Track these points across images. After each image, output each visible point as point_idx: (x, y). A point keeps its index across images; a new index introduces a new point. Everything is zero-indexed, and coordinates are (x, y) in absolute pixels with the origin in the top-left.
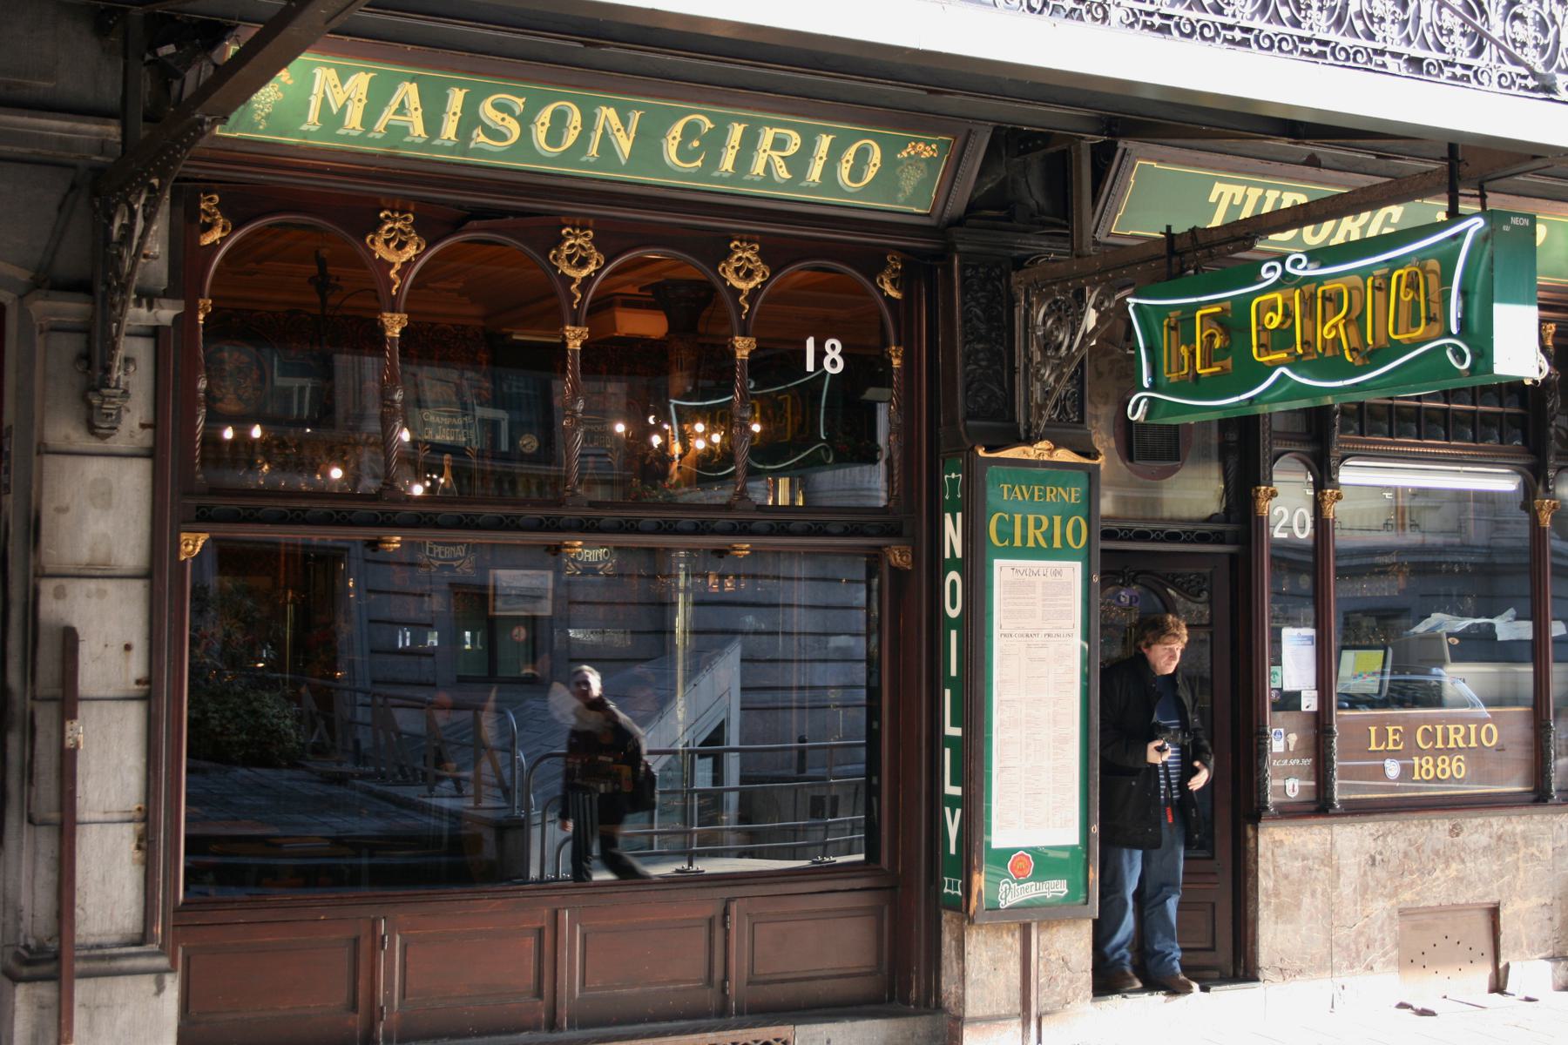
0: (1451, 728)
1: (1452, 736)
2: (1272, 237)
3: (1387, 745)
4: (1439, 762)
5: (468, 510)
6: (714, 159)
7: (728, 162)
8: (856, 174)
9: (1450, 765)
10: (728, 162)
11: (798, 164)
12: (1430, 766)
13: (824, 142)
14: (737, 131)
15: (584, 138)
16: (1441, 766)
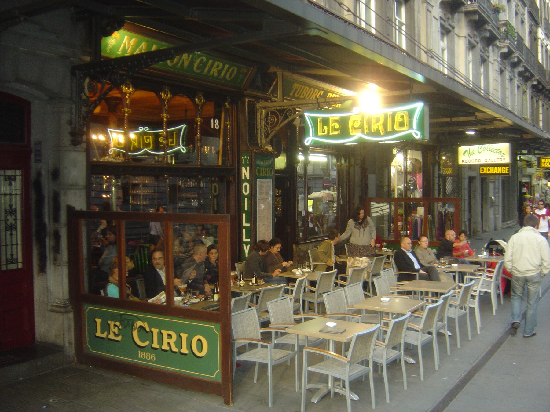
0: (165, 333)
1: (166, 340)
2: (540, 61)
3: (109, 333)
4: (142, 353)
5: (236, 352)
6: (203, 70)
7: (206, 70)
8: (230, 76)
9: (150, 356)
10: (206, 70)
11: (220, 72)
12: (144, 355)
13: (227, 66)
14: (210, 62)
15: (178, 63)
16: (142, 355)
